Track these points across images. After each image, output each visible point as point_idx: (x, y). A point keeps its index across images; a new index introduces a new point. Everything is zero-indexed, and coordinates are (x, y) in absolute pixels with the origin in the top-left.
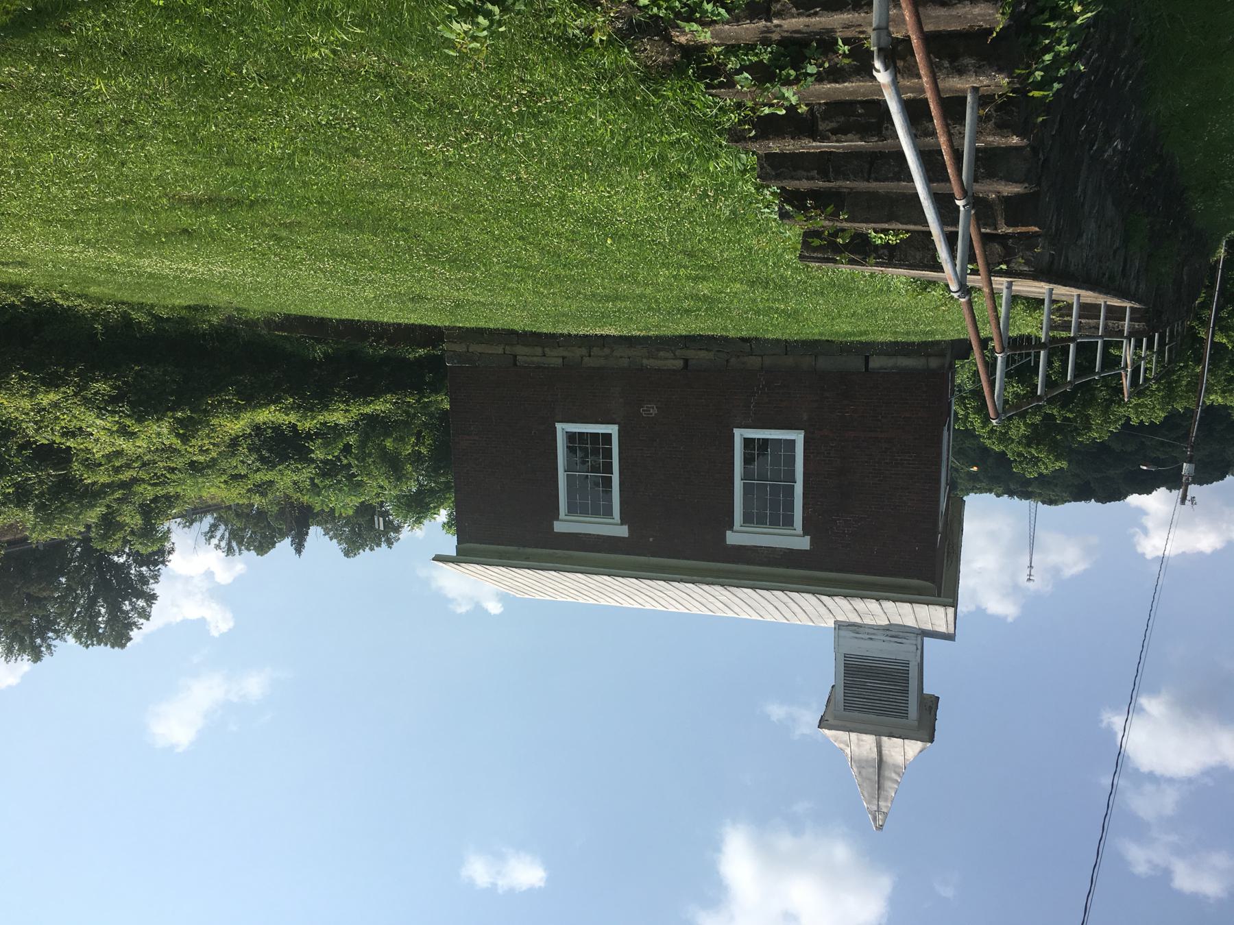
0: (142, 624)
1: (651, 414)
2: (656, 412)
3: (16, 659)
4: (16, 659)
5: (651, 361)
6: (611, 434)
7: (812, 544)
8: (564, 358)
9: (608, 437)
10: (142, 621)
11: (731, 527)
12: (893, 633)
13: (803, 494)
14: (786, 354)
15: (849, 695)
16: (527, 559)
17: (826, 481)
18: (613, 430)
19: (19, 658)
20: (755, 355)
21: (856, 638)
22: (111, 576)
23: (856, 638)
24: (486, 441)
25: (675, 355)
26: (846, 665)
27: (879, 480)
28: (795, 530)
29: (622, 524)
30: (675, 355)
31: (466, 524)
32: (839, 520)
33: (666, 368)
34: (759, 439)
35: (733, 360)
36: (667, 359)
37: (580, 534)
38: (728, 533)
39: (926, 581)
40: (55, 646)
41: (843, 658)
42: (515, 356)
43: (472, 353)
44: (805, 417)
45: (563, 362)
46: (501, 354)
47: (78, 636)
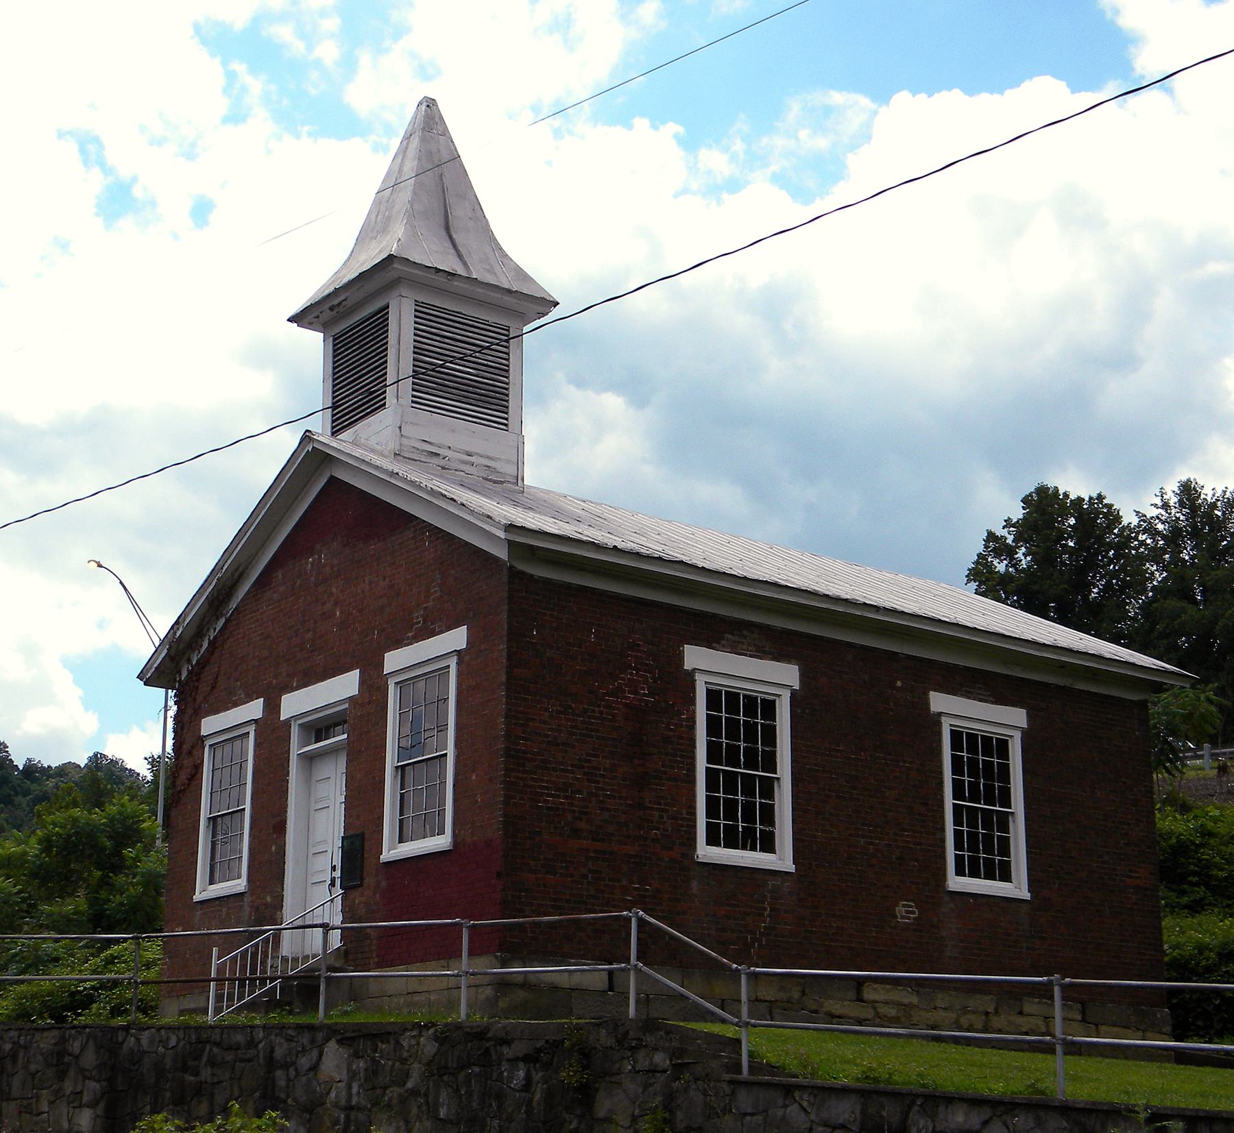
0: (1004, 528)
1: (904, 906)
2: (897, 908)
3: (1225, 492)
4: (1225, 492)
5: (906, 1001)
6: (707, 845)
7: (680, 657)
8: (1021, 1013)
9: (712, 840)
10: (1000, 532)
11: (794, 695)
12: (435, 461)
13: (695, 747)
14: (723, 1000)
15: (501, 355)
16: (1063, 666)
17: (663, 766)
18: (706, 852)
19: (1219, 493)
20: (765, 1001)
21: (489, 458)
22: (1122, 625)
23: (489, 458)
24: (1116, 875)
25: (875, 1008)
26: (505, 409)
27: (589, 761)
28: (706, 683)
29: (940, 714)
30: (875, 1008)
31: (1137, 733)
32: (644, 695)
33: (888, 987)
34: (753, 849)
35: (796, 995)
36: (886, 1003)
37: (993, 703)
38: (797, 687)
39: (523, 573)
40: (1155, 506)
41: (510, 423)
42: (1084, 1020)
43: (1138, 1029)
44: (695, 885)
45: (1022, 1007)
46: (1102, 1025)
47: (1113, 517)
